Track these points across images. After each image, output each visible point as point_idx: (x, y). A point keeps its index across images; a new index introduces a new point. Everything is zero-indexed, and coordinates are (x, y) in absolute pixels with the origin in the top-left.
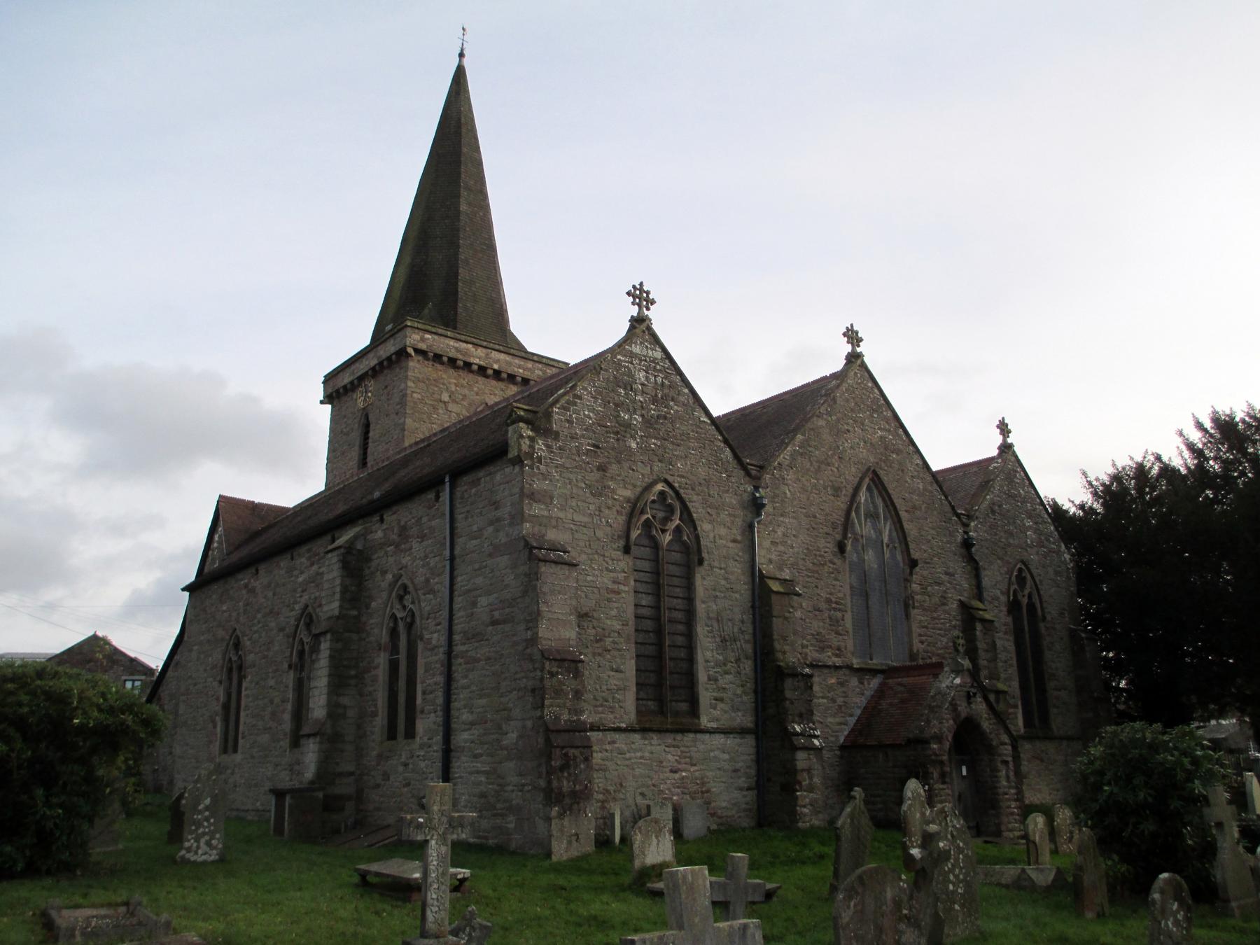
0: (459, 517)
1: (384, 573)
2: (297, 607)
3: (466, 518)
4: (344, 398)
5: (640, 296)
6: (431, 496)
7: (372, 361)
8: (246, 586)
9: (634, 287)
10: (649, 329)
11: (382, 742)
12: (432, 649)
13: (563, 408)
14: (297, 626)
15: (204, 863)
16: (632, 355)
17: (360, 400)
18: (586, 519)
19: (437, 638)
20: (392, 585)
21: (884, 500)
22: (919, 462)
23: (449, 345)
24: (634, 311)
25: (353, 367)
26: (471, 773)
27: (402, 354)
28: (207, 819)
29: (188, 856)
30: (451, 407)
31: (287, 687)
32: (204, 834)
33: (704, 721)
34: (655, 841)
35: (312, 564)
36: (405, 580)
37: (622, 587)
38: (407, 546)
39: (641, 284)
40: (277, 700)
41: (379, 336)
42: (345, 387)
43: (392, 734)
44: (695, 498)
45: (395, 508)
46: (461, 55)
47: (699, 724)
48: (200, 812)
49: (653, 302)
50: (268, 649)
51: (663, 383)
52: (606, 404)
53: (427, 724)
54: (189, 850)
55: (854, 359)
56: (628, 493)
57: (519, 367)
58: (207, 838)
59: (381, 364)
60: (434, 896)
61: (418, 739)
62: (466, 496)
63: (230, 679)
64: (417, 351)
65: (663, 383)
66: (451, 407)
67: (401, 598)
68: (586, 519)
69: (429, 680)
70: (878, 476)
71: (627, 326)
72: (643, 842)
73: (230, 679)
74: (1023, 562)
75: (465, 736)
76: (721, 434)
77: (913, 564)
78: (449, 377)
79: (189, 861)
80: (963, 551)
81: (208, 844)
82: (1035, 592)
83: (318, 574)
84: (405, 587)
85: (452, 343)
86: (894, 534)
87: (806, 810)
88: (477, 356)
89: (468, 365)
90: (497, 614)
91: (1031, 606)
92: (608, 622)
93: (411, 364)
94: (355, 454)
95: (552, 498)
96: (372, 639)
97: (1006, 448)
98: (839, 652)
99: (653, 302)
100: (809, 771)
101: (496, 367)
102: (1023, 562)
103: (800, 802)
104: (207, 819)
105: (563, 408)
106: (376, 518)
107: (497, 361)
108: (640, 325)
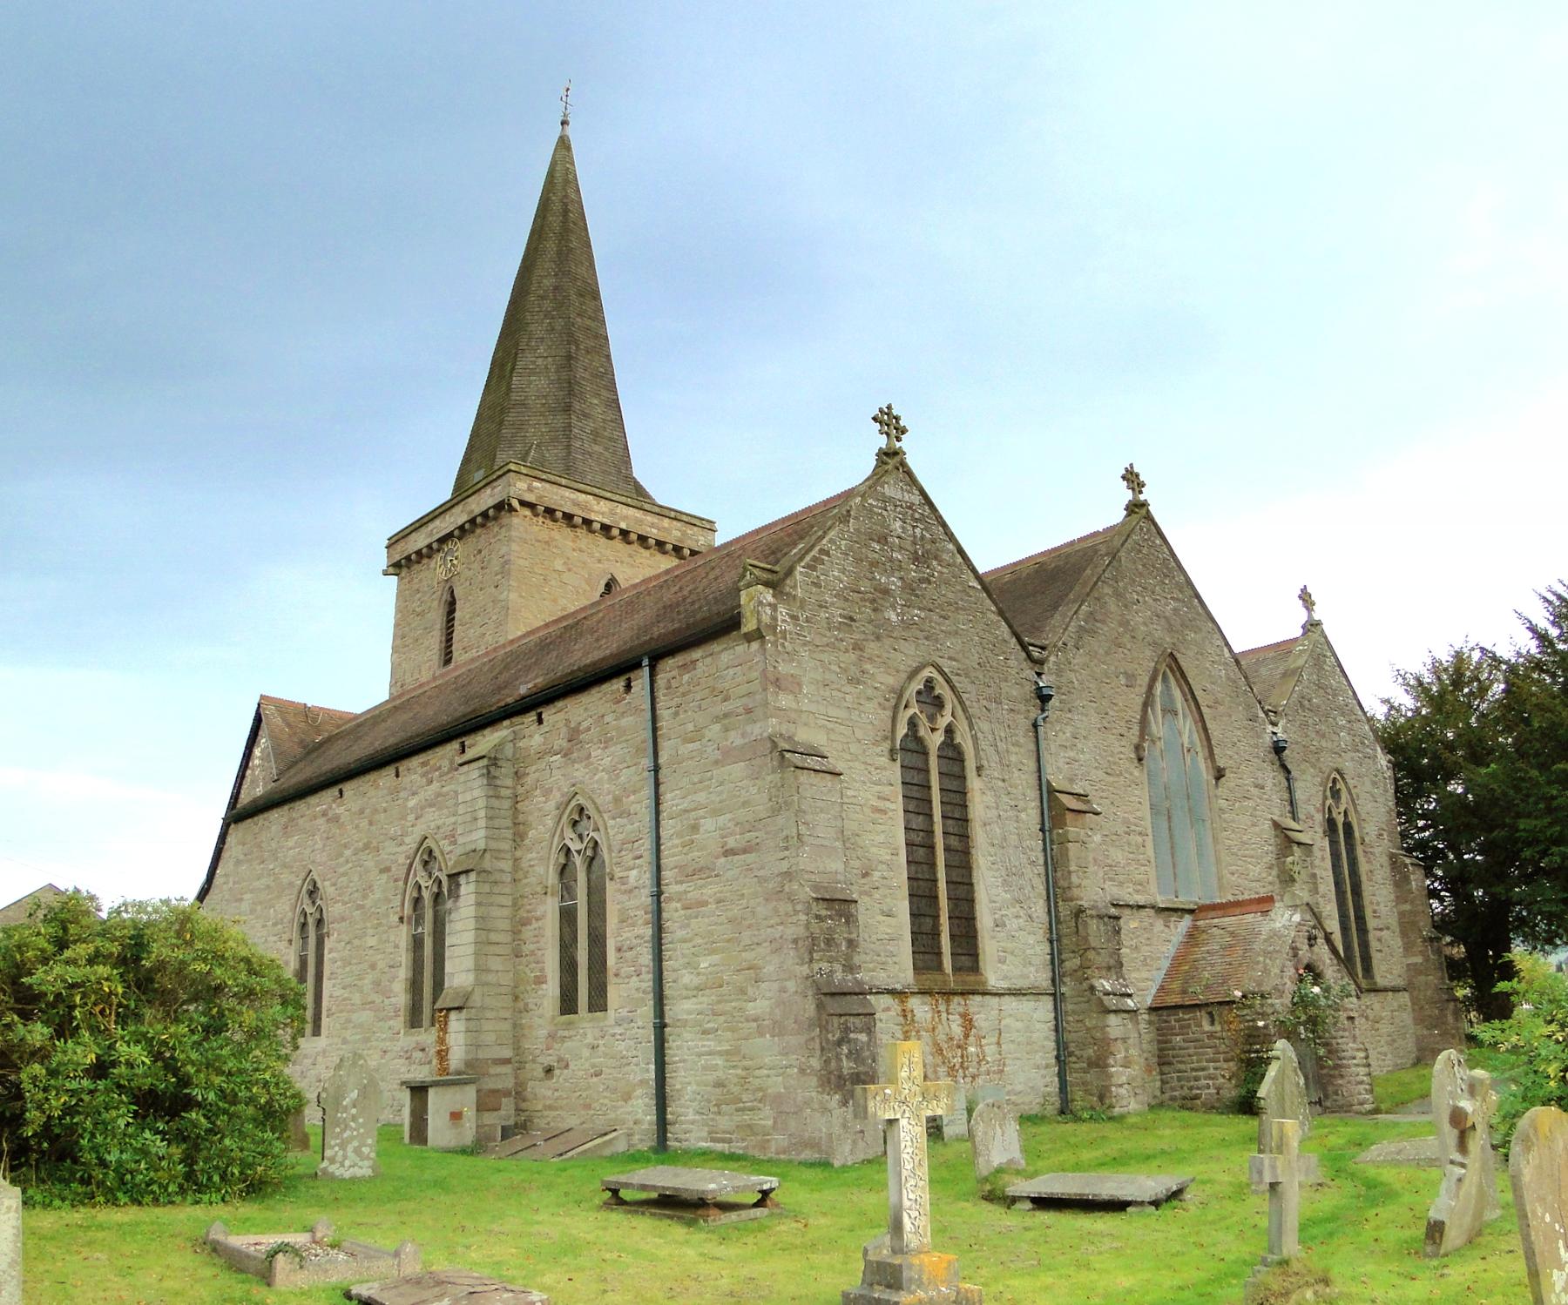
0: (664, 713)
1: (547, 793)
2: (407, 840)
3: (676, 714)
4: (416, 567)
5: (889, 422)
6: (618, 684)
7: (458, 517)
8: (324, 814)
9: (881, 410)
10: (903, 464)
11: (553, 1018)
12: (631, 891)
13: (808, 566)
14: (411, 865)
15: (353, 1180)
16: (885, 500)
17: (436, 570)
18: (842, 714)
19: (639, 876)
20: (562, 807)
21: (1184, 695)
22: (1220, 643)
23: (563, 498)
24: (882, 442)
25: (431, 526)
26: (699, 1055)
27: (503, 507)
28: (354, 1118)
29: (332, 1168)
30: (566, 577)
31: (396, 946)
32: (352, 1138)
33: (993, 975)
34: (999, 1131)
35: (430, 782)
36: (581, 800)
37: (888, 804)
38: (583, 754)
39: (889, 407)
40: (381, 965)
41: (463, 489)
42: (419, 553)
43: (568, 1004)
44: (970, 687)
45: (560, 704)
46: (564, 123)
47: (984, 983)
48: (345, 1109)
49: (904, 431)
50: (365, 897)
51: (923, 537)
52: (858, 561)
53: (628, 988)
54: (332, 1160)
55: (1137, 508)
56: (891, 680)
57: (652, 525)
58: (355, 1143)
59: (472, 521)
60: (912, 1196)
61: (611, 1012)
62: (674, 684)
63: (304, 938)
64: (523, 503)
65: (923, 537)
66: (566, 577)
67: (575, 824)
68: (842, 714)
69: (626, 933)
70: (1175, 660)
71: (872, 463)
72: (986, 1133)
73: (304, 938)
74: (1338, 771)
75: (687, 1005)
76: (996, 605)
77: (1219, 774)
78: (561, 535)
79: (332, 1177)
80: (1273, 756)
81: (357, 1151)
82: (1351, 809)
83: (439, 795)
84: (581, 810)
85: (567, 493)
86: (1195, 736)
87: (1123, 1091)
88: (600, 511)
89: (587, 522)
90: (731, 843)
91: (1348, 826)
92: (874, 850)
93: (515, 521)
94: (435, 641)
95: (800, 685)
96: (532, 880)
97: (1312, 626)
98: (1141, 885)
99: (904, 431)
100: (1124, 1040)
101: (623, 526)
102: (1338, 771)
103: (1114, 1080)
104: (354, 1118)
105: (808, 566)
106: (532, 716)
107: (625, 518)
108: (890, 459)
